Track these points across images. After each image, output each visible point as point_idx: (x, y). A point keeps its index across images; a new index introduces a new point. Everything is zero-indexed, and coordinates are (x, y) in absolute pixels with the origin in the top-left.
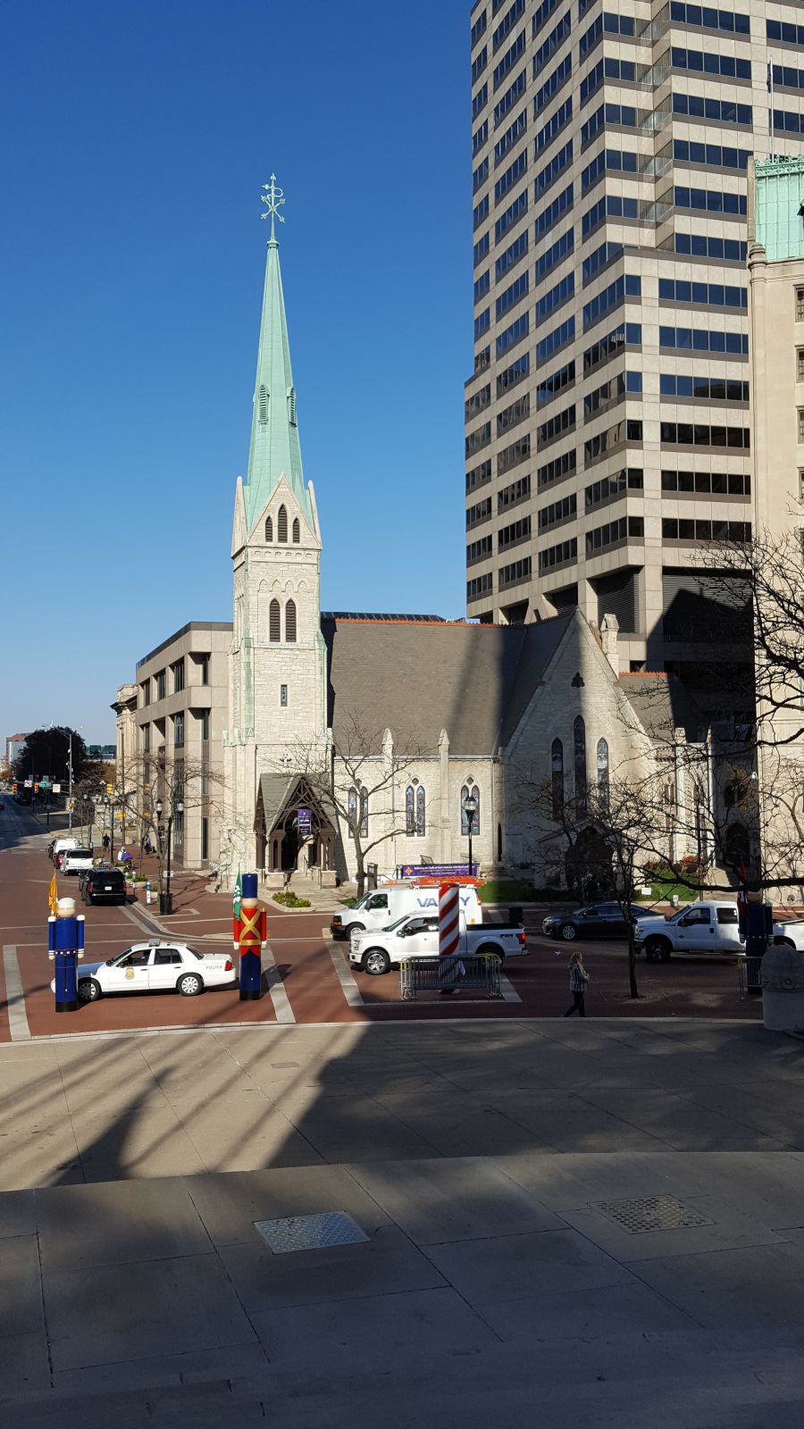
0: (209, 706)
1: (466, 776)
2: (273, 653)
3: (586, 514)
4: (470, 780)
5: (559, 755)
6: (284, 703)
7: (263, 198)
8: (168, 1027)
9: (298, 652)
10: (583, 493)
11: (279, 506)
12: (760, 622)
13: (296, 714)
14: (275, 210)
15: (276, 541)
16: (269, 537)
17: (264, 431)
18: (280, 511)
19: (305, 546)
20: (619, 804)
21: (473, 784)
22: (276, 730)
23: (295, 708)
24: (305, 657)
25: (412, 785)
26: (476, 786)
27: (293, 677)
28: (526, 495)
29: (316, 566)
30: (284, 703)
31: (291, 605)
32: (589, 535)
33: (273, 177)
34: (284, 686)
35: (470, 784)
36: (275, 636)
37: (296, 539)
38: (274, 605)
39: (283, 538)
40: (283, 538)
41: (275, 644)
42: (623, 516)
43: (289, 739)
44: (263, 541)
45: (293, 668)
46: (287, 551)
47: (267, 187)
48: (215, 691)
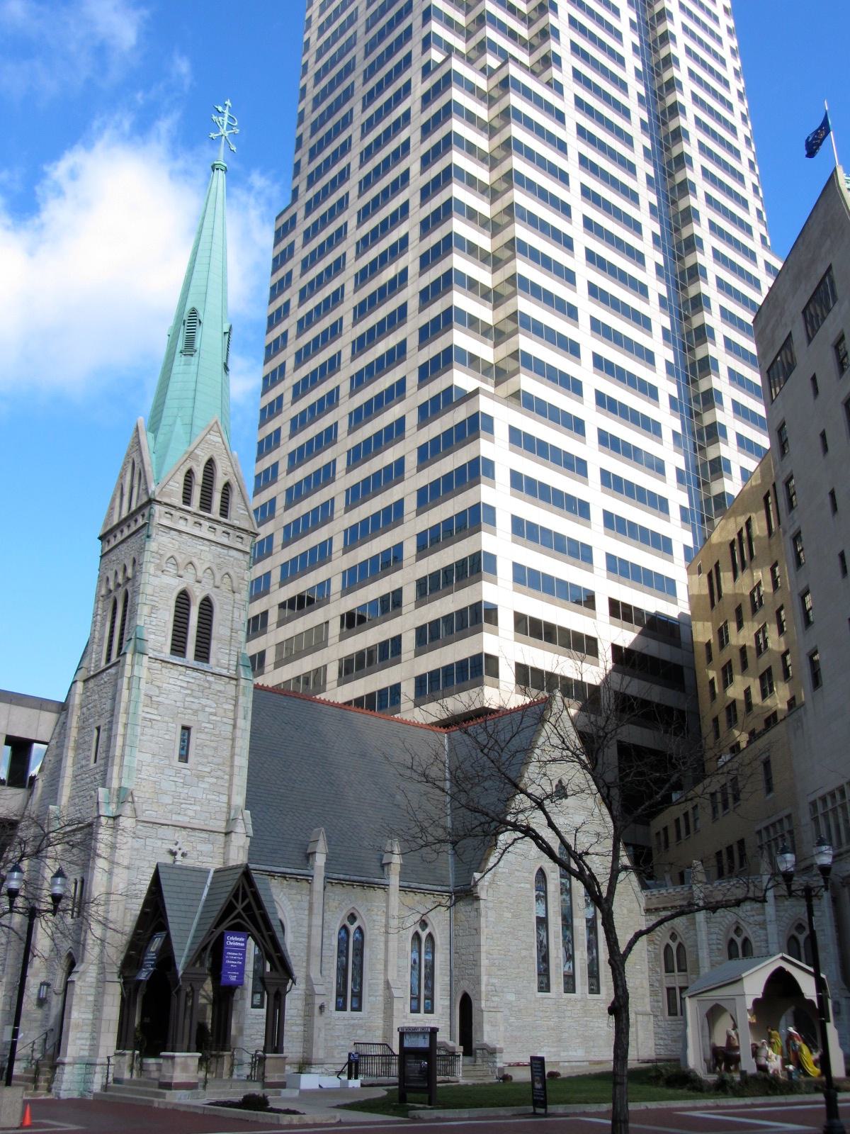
1: (345, 912)
3: (338, 686)
4: (352, 918)
5: (542, 894)
6: (184, 758)
7: (214, 117)
9: (211, 679)
10: (413, 634)
11: (206, 459)
13: (200, 777)
14: (227, 135)
15: (195, 506)
16: (187, 499)
18: (207, 464)
21: (743, 937)
22: (167, 799)
23: (200, 768)
24: (221, 688)
25: (796, 934)
26: (359, 928)
27: (201, 716)
28: (397, 610)
29: (247, 557)
30: (184, 758)
31: (207, 605)
33: (228, 103)
35: (423, 930)
36: (178, 647)
38: (183, 599)
39: (206, 504)
40: (206, 504)
42: (476, 652)
43: (187, 819)
44: (178, 501)
45: (204, 701)
46: (210, 524)
47: (220, 109)
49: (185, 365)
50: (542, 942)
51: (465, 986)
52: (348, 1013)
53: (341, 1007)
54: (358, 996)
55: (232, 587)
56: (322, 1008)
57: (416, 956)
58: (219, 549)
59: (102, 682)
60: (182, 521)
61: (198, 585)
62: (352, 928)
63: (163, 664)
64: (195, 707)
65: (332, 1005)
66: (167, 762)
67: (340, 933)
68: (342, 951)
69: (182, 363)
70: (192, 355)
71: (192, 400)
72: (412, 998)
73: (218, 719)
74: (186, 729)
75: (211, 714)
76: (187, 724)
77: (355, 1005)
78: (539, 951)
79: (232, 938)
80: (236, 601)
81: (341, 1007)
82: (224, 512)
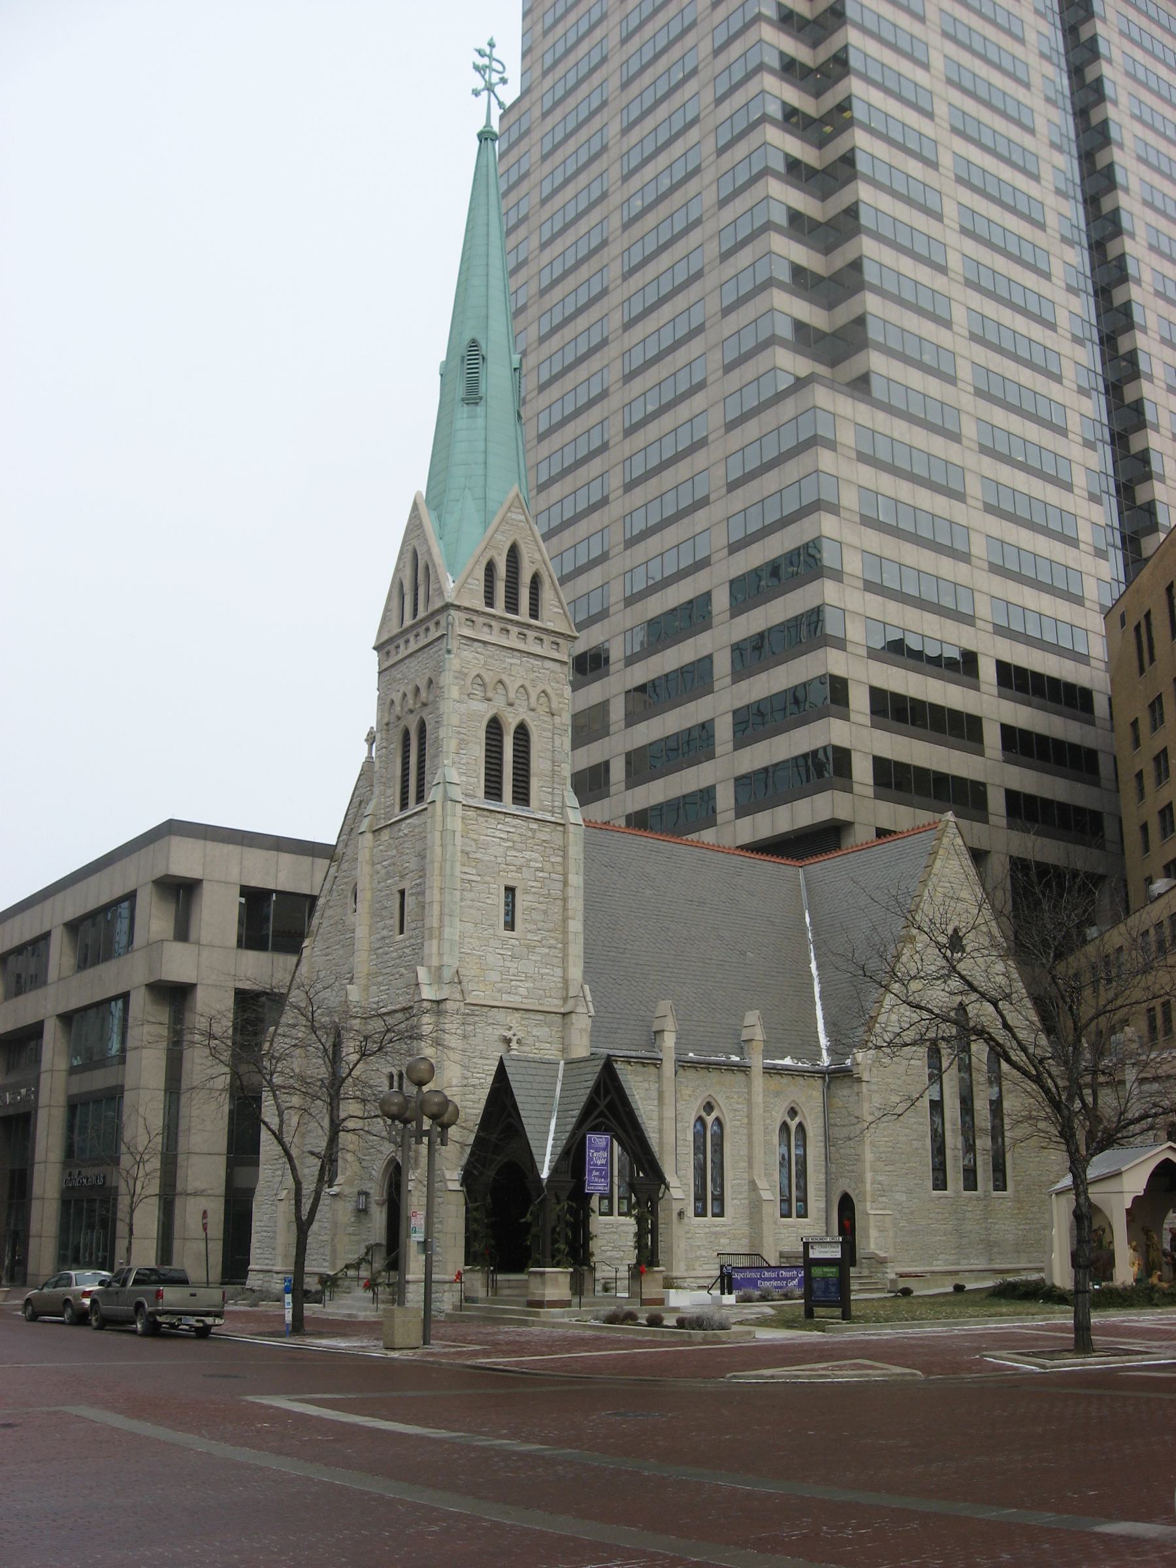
0: (194, 982)
2: (492, 822)
4: (709, 1107)
6: (510, 925)
8: (1127, 1340)
9: (534, 826)
12: (325, 1050)
15: (499, 609)
17: (472, 417)
19: (550, 626)
20: (869, 1062)
27: (526, 873)
30: (510, 925)
31: (522, 732)
32: (629, 757)
34: (510, 890)
36: (493, 790)
37: (534, 614)
38: (494, 727)
39: (512, 605)
40: (512, 605)
41: (492, 805)
43: (519, 999)
44: (479, 603)
48: (205, 953)
49: (468, 418)
50: (936, 1130)
51: (844, 1185)
52: (709, 1219)
53: (700, 1213)
54: (719, 1199)
55: (550, 708)
56: (681, 1214)
57: (784, 1150)
58: (532, 661)
59: (401, 834)
60: (486, 629)
61: (510, 709)
62: (710, 1119)
63: (479, 812)
64: (519, 862)
65: (690, 1211)
66: (491, 931)
67: (695, 1126)
68: (699, 1148)
69: (465, 416)
70: (477, 403)
71: (483, 466)
72: (781, 1200)
73: (546, 875)
74: (510, 890)
75: (537, 869)
76: (511, 883)
77: (717, 1211)
78: (933, 1140)
80: (556, 725)
81: (700, 1213)
82: (534, 614)
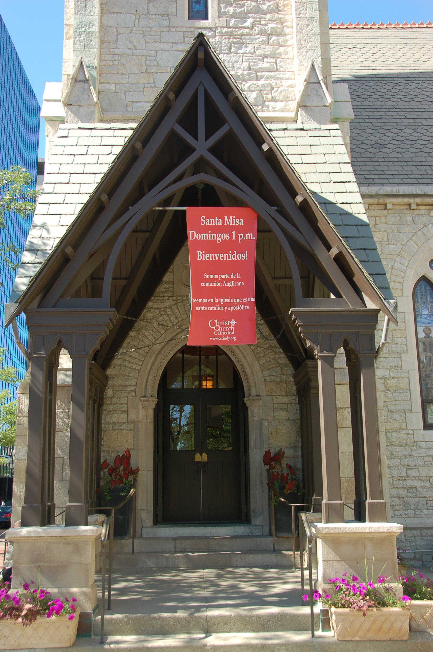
79: (205, 222)
